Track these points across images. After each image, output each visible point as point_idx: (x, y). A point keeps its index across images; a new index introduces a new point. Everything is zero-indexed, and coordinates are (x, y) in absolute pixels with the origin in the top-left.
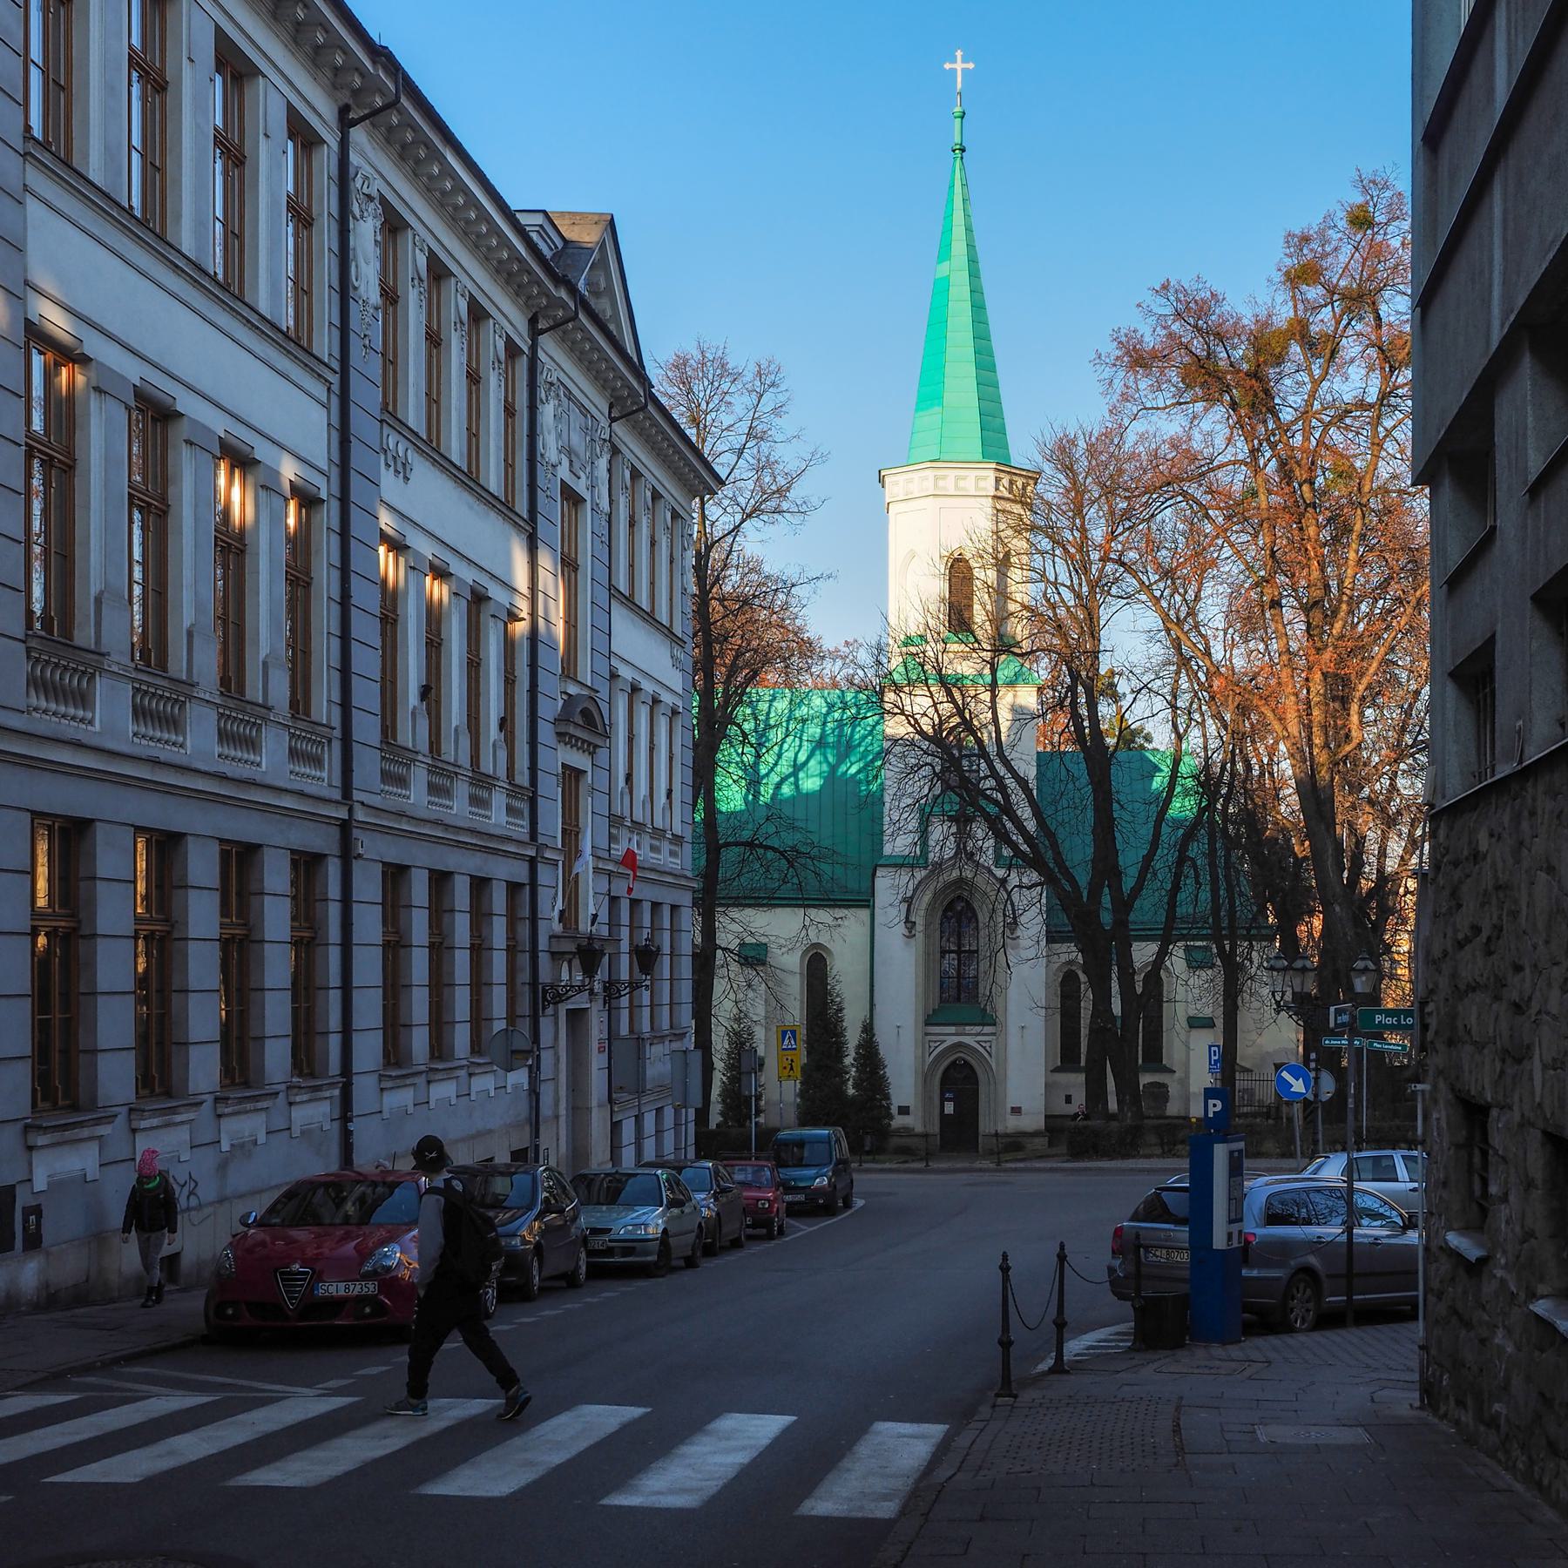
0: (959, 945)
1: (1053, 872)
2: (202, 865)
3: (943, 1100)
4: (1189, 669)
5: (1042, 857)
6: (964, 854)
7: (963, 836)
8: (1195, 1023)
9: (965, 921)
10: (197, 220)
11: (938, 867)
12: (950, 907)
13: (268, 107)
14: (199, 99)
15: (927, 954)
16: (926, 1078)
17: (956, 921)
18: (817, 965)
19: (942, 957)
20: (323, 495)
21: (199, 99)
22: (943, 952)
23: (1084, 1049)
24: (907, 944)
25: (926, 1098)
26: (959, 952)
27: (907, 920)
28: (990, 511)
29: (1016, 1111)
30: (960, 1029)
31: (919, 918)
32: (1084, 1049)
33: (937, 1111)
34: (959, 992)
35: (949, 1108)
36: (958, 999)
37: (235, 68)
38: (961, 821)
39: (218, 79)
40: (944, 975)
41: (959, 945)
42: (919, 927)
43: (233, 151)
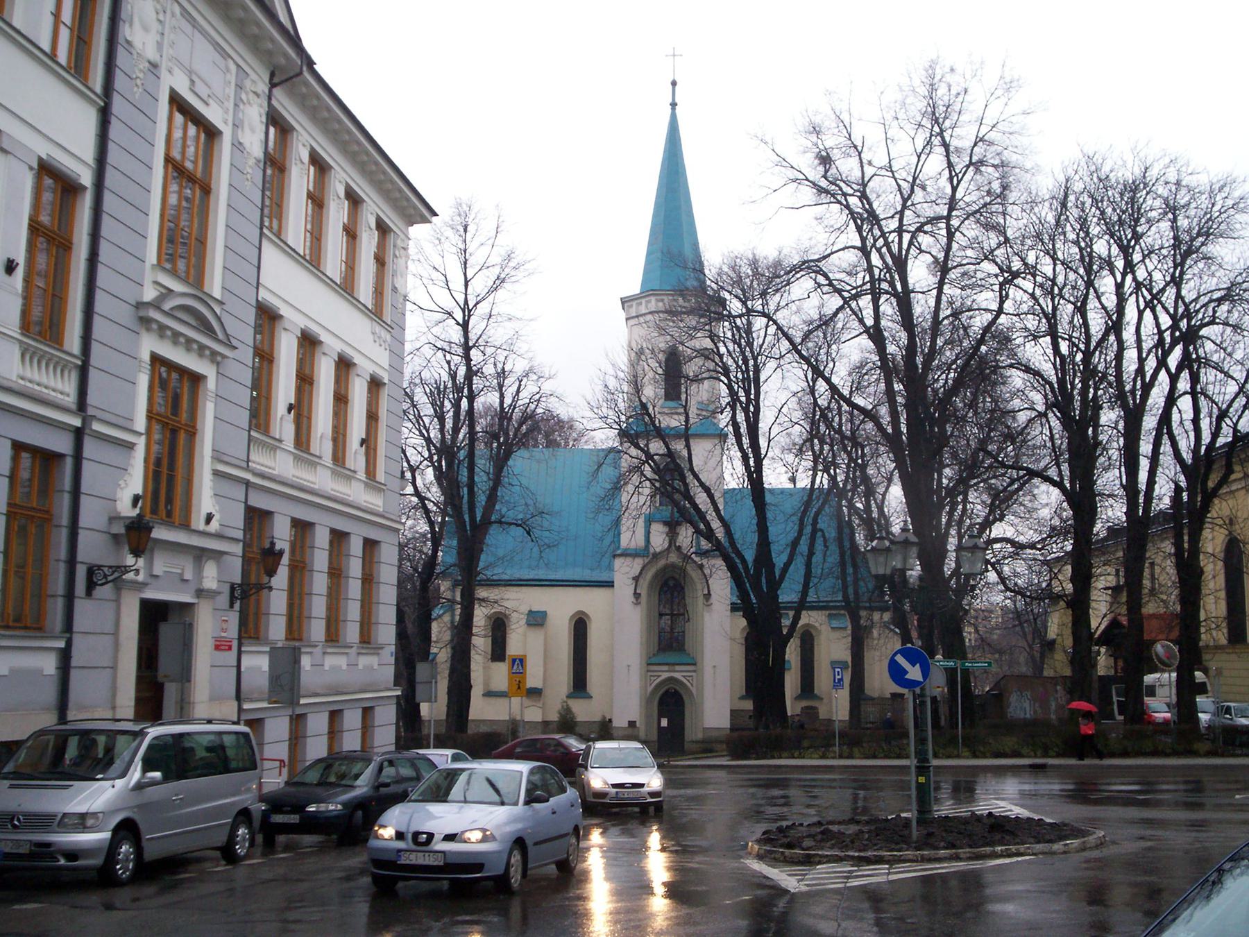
0: (672, 609)
2: (356, 547)
3: (660, 716)
4: (1071, 269)
5: (728, 553)
10: (333, 264)
11: (656, 556)
12: (665, 584)
13: (300, 152)
14: (337, 213)
15: (649, 616)
16: (648, 701)
17: (670, 591)
18: (580, 626)
20: (386, 381)
21: (337, 213)
22: (661, 615)
25: (648, 716)
26: (672, 615)
27: (635, 593)
31: (643, 590)
33: (655, 725)
34: (670, 637)
35: (664, 723)
37: (354, 199)
38: (672, 527)
39: (312, 168)
40: (661, 631)
41: (672, 609)
43: (351, 233)
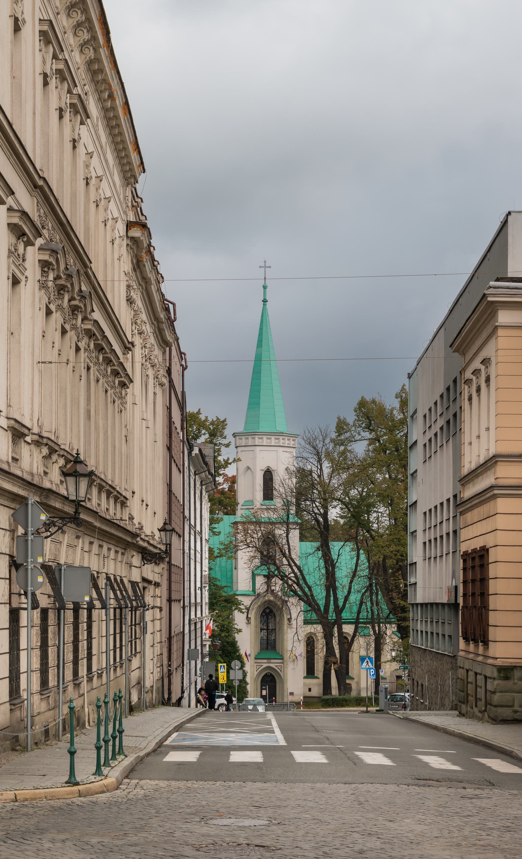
0: (268, 626)
1: (309, 601)
3: (262, 689)
6: (269, 590)
7: (268, 584)
8: (362, 659)
9: (270, 617)
12: (264, 611)
19: (261, 631)
22: (262, 630)
23: (331, 592)
24: (247, 626)
28: (37, 752)
29: (292, 694)
30: (269, 661)
32: (331, 592)
36: (267, 649)
40: (262, 639)
42: (252, 620)
